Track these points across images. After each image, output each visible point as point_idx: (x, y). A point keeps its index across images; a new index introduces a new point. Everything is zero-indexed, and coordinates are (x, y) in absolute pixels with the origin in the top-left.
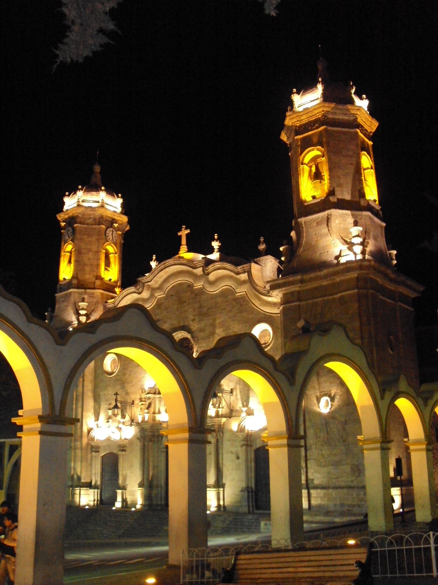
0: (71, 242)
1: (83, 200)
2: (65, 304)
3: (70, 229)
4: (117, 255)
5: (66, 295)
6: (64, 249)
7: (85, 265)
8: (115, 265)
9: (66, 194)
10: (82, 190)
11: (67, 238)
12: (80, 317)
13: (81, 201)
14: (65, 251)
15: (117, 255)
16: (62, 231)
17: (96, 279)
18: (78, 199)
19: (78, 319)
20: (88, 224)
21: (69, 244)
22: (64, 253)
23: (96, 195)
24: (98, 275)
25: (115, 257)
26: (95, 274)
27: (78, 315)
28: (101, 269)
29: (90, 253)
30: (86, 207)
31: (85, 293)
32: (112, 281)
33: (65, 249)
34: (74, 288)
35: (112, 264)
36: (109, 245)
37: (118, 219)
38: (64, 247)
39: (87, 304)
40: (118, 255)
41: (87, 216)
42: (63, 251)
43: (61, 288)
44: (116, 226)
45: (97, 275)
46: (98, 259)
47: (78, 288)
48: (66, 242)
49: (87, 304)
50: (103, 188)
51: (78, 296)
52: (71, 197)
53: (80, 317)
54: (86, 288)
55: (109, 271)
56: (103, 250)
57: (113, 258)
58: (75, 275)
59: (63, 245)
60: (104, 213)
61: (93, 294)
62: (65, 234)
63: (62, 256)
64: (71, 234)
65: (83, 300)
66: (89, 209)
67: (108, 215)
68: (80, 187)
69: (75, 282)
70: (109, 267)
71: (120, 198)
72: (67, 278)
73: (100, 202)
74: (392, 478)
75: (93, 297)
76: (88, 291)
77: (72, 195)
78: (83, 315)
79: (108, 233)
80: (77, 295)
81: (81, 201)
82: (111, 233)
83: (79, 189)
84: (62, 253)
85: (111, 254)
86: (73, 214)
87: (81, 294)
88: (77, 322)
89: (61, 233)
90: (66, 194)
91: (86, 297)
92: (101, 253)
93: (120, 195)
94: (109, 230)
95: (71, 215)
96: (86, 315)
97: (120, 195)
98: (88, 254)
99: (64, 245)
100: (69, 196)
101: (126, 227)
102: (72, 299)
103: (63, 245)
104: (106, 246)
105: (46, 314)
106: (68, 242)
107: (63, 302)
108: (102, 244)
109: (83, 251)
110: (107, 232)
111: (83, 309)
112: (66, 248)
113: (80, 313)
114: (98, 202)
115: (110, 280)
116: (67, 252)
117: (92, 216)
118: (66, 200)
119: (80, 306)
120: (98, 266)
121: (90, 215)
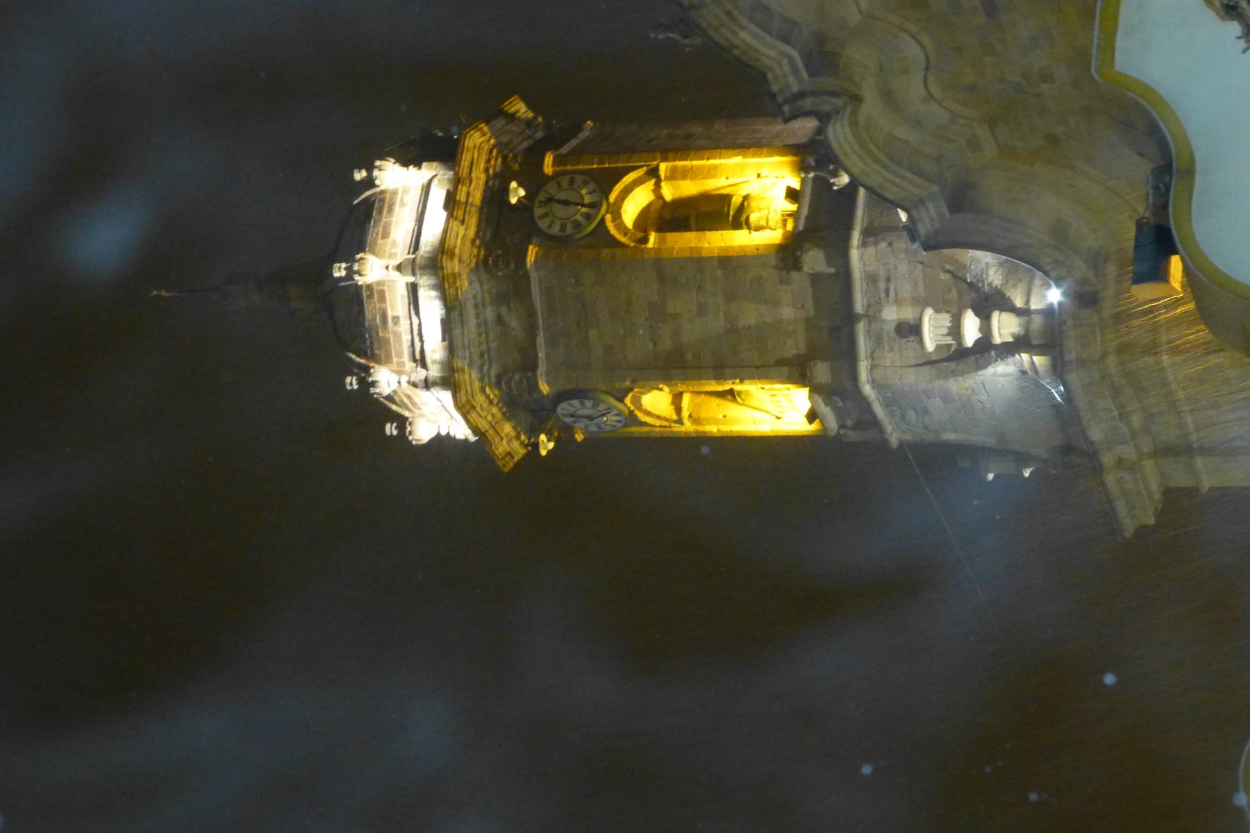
0: (628, 400)
1: (415, 360)
2: (936, 404)
3: (563, 408)
4: (663, 167)
5: (888, 404)
6: (665, 423)
7: (732, 330)
8: (711, 173)
9: (395, 433)
10: (367, 369)
11: (611, 419)
12: (997, 340)
13: (421, 374)
14: (675, 417)
15: (663, 167)
16: (579, 437)
17: (797, 266)
18: (415, 385)
19: (1009, 349)
20: (531, 331)
21: (639, 407)
22: (686, 421)
23: (382, 298)
24: (773, 262)
25: (673, 175)
26: (770, 274)
27: (985, 349)
28: (742, 248)
29: (673, 306)
30: (451, 350)
31: (873, 316)
32: (796, 185)
33: (667, 420)
34: (854, 377)
35: (714, 184)
36: (617, 216)
37: (483, 177)
38: (658, 423)
39: (929, 312)
40: (665, 159)
41: (491, 336)
42: (677, 428)
43: (859, 426)
44: (522, 193)
45: (776, 267)
46: (698, 262)
47: (850, 356)
48: (632, 419)
49: (929, 312)
50: (339, 271)
51: (892, 350)
52: (407, 408)
53: (997, 340)
54: (851, 318)
55: (746, 198)
56: (651, 244)
57: (681, 183)
58: (785, 370)
59: (646, 429)
60: (466, 257)
61: (872, 279)
62: (593, 428)
63: (701, 428)
64: (589, 403)
65: (911, 330)
66: (457, 332)
67: (472, 232)
68: (352, 383)
69: (822, 371)
70: (726, 199)
71: (376, 173)
72: (806, 405)
73: (411, 279)
74: (1175, 252)
75: (888, 280)
76: (859, 307)
77: (394, 407)
78: (986, 329)
79: (563, 227)
80: (888, 358)
81: (421, 374)
82: (559, 210)
83: (367, 385)
84: (683, 429)
85: (659, 196)
86: (491, 402)
87: (877, 339)
88: (1025, 357)
89: (590, 441)
90: (395, 433)
91: (891, 314)
92: (665, 255)
93: (359, 175)
94: (543, 224)
95: (494, 410)
96: (984, 316)
97: (359, 175)
98: (676, 316)
99: (645, 424)
100: (402, 422)
101: (512, 117)
102: (915, 379)
103: (646, 429)
104: (625, 232)
105: (991, 476)
106: (631, 412)
107: (926, 411)
108: (618, 251)
109: (667, 344)
110: (555, 230)
111: (956, 330)
112: (659, 417)
113: (977, 342)
114: (413, 289)
115: (792, 195)
116: (678, 410)
117: (490, 313)
118: (422, 433)
119: (939, 348)
120: (730, 263)
121: (482, 324)
